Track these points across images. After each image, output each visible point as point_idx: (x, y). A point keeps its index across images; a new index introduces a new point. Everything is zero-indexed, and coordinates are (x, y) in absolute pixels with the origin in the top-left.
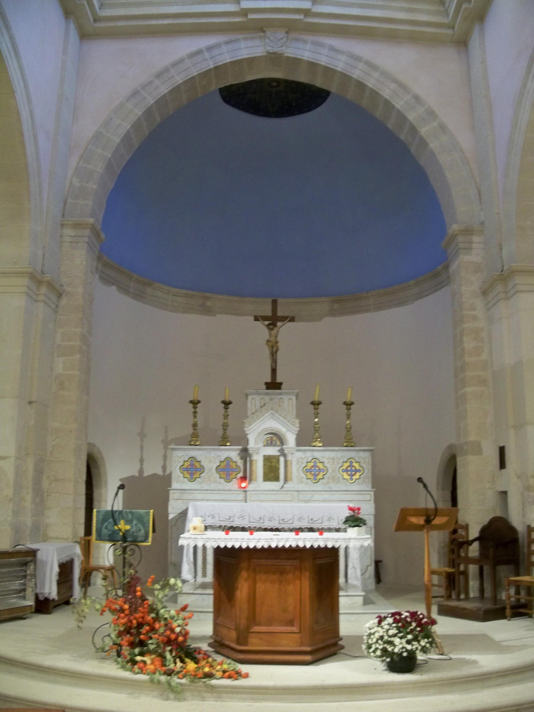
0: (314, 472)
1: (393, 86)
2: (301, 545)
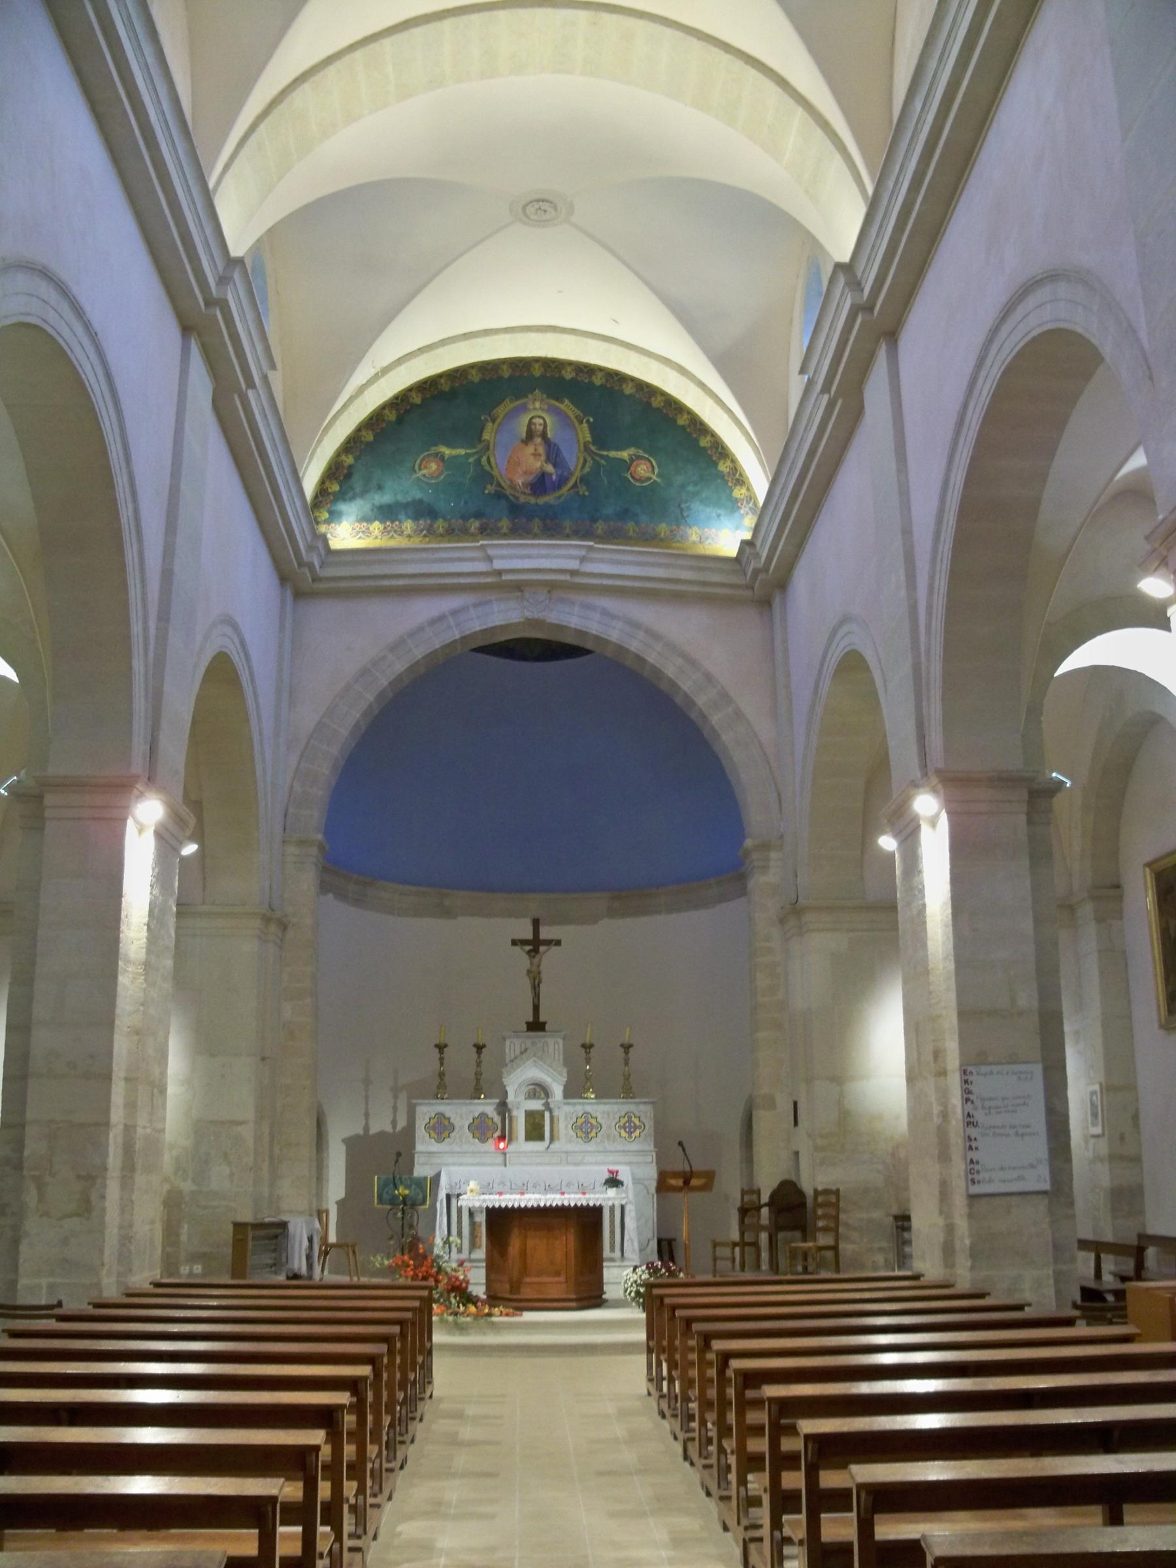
0: (586, 1129)
1: (680, 661)
2: (566, 1204)
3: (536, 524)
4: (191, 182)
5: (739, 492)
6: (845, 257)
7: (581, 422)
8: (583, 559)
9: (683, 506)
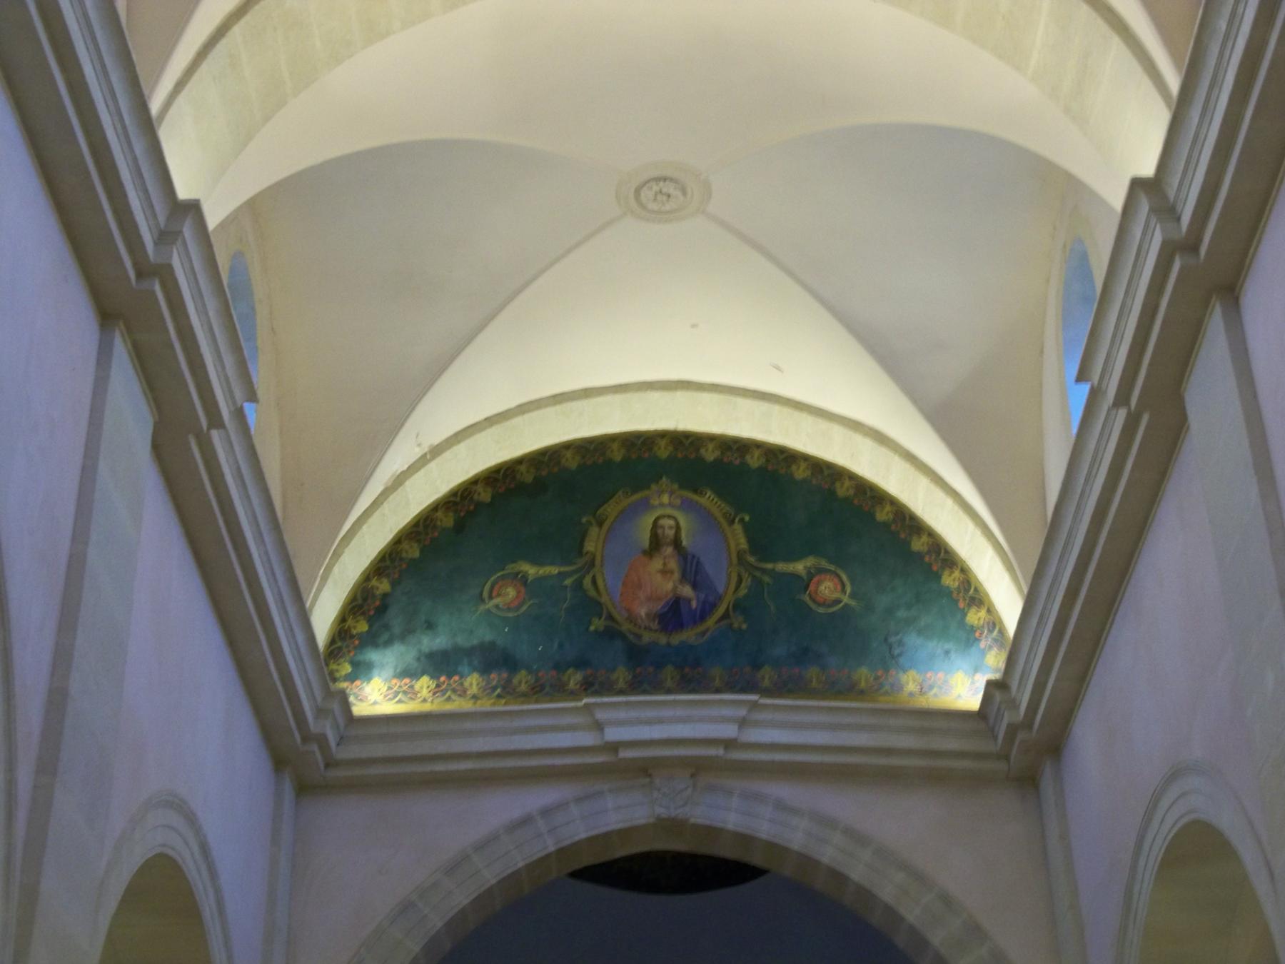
3: (669, 673)
4: (132, 130)
5: (975, 617)
6: (1148, 168)
7: (732, 522)
8: (743, 723)
9: (893, 639)
